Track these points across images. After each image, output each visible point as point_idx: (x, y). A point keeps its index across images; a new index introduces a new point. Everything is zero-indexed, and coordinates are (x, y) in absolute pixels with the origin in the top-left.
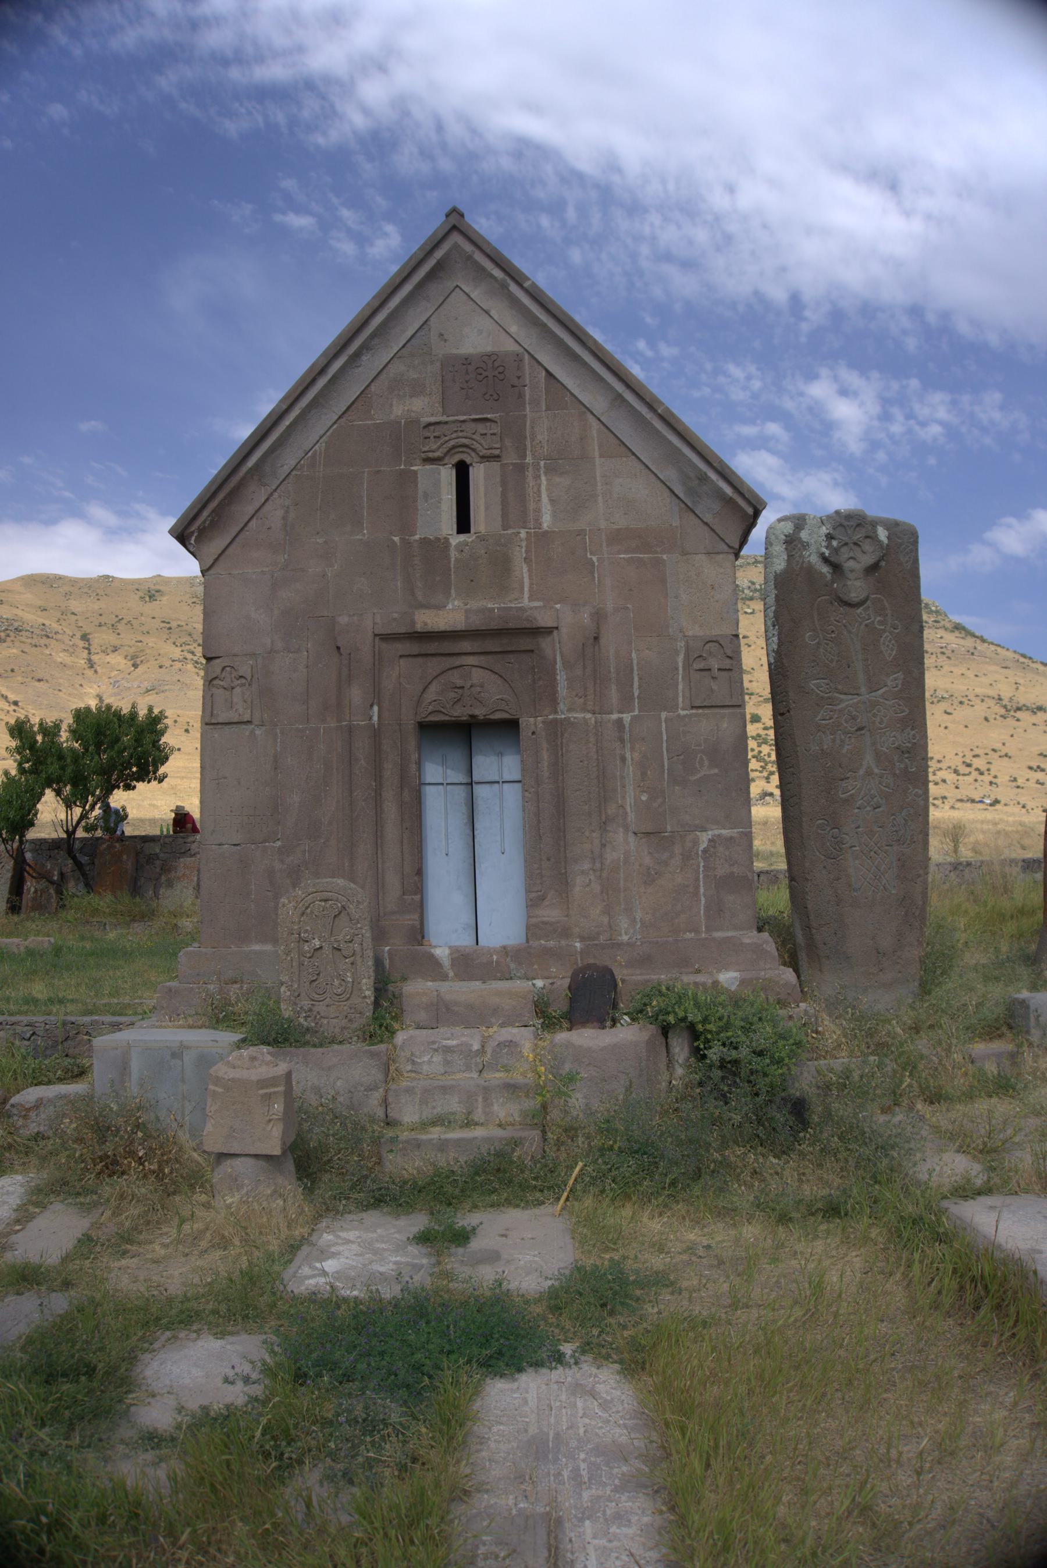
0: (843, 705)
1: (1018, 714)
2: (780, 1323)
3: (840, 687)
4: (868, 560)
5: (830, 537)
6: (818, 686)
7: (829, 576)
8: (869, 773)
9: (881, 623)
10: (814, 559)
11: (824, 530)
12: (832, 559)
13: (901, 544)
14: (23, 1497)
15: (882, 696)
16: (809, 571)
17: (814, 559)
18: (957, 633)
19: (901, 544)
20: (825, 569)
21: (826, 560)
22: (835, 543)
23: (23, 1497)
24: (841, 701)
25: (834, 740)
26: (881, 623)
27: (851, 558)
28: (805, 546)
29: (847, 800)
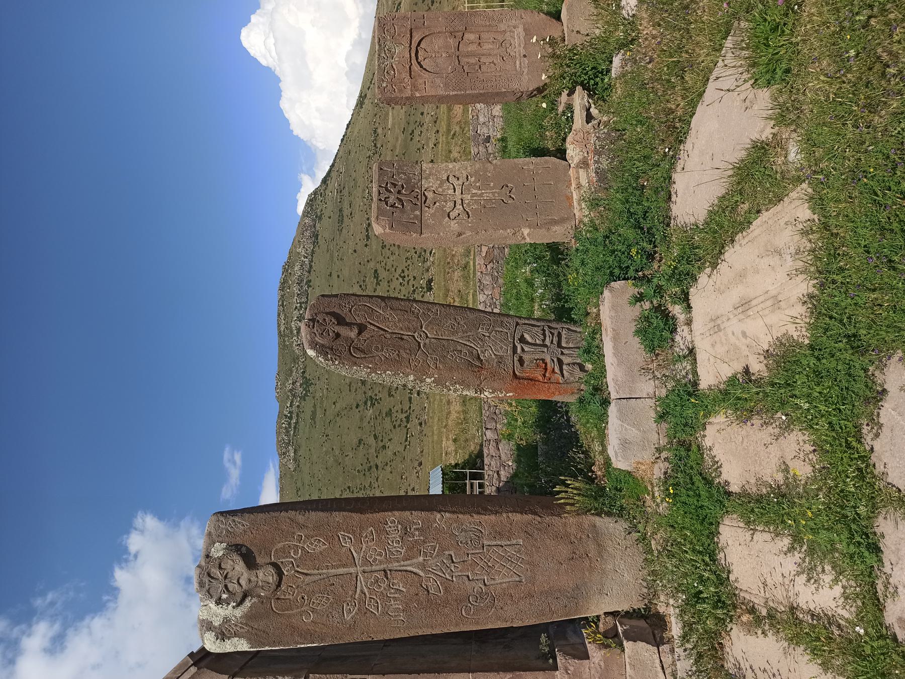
0: (366, 590)
1: (379, 146)
2: (587, 573)
3: (350, 593)
4: (240, 566)
5: (219, 602)
6: (350, 611)
7: (254, 600)
8: (423, 566)
9: (296, 553)
10: (239, 613)
11: (212, 605)
12: (239, 600)
13: (227, 531)
14: (593, 105)
15: (358, 553)
16: (249, 617)
17: (239, 613)
18: (329, 182)
19: (227, 531)
20: (248, 603)
21: (240, 604)
22: (224, 596)
23: (593, 105)
24: (362, 592)
25: (395, 599)
26: (296, 553)
27: (238, 581)
28: (226, 620)
29: (446, 589)
